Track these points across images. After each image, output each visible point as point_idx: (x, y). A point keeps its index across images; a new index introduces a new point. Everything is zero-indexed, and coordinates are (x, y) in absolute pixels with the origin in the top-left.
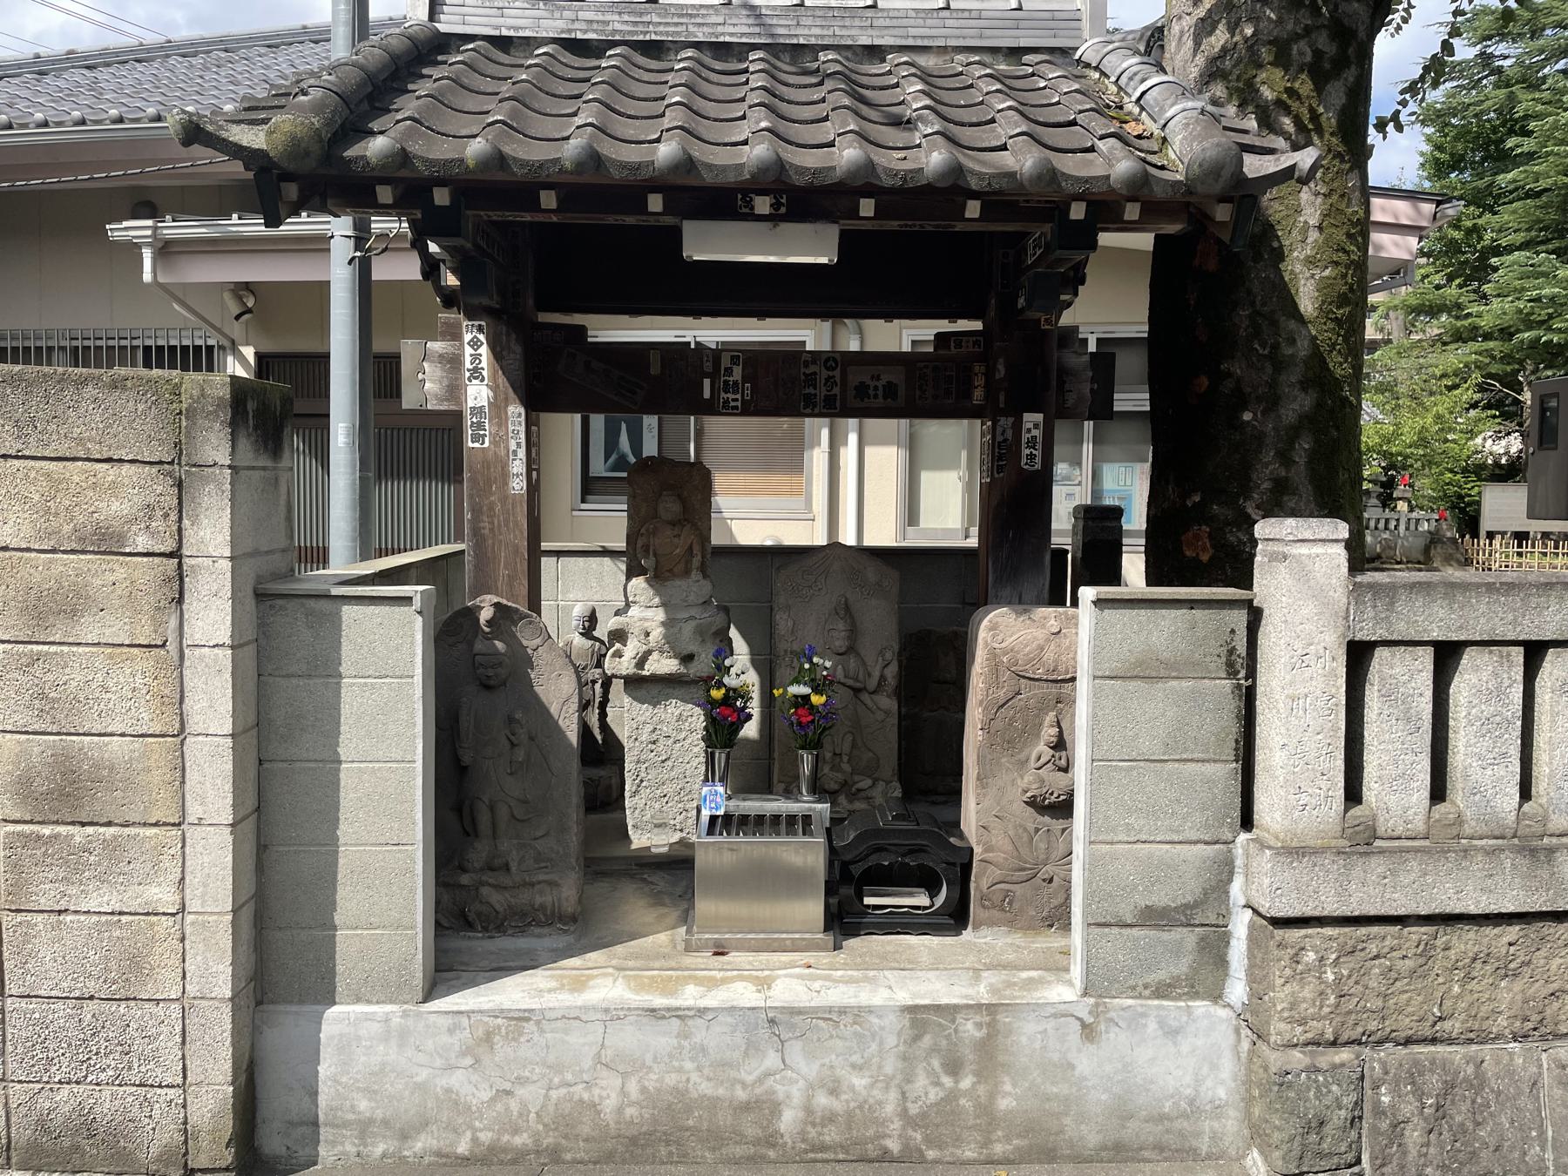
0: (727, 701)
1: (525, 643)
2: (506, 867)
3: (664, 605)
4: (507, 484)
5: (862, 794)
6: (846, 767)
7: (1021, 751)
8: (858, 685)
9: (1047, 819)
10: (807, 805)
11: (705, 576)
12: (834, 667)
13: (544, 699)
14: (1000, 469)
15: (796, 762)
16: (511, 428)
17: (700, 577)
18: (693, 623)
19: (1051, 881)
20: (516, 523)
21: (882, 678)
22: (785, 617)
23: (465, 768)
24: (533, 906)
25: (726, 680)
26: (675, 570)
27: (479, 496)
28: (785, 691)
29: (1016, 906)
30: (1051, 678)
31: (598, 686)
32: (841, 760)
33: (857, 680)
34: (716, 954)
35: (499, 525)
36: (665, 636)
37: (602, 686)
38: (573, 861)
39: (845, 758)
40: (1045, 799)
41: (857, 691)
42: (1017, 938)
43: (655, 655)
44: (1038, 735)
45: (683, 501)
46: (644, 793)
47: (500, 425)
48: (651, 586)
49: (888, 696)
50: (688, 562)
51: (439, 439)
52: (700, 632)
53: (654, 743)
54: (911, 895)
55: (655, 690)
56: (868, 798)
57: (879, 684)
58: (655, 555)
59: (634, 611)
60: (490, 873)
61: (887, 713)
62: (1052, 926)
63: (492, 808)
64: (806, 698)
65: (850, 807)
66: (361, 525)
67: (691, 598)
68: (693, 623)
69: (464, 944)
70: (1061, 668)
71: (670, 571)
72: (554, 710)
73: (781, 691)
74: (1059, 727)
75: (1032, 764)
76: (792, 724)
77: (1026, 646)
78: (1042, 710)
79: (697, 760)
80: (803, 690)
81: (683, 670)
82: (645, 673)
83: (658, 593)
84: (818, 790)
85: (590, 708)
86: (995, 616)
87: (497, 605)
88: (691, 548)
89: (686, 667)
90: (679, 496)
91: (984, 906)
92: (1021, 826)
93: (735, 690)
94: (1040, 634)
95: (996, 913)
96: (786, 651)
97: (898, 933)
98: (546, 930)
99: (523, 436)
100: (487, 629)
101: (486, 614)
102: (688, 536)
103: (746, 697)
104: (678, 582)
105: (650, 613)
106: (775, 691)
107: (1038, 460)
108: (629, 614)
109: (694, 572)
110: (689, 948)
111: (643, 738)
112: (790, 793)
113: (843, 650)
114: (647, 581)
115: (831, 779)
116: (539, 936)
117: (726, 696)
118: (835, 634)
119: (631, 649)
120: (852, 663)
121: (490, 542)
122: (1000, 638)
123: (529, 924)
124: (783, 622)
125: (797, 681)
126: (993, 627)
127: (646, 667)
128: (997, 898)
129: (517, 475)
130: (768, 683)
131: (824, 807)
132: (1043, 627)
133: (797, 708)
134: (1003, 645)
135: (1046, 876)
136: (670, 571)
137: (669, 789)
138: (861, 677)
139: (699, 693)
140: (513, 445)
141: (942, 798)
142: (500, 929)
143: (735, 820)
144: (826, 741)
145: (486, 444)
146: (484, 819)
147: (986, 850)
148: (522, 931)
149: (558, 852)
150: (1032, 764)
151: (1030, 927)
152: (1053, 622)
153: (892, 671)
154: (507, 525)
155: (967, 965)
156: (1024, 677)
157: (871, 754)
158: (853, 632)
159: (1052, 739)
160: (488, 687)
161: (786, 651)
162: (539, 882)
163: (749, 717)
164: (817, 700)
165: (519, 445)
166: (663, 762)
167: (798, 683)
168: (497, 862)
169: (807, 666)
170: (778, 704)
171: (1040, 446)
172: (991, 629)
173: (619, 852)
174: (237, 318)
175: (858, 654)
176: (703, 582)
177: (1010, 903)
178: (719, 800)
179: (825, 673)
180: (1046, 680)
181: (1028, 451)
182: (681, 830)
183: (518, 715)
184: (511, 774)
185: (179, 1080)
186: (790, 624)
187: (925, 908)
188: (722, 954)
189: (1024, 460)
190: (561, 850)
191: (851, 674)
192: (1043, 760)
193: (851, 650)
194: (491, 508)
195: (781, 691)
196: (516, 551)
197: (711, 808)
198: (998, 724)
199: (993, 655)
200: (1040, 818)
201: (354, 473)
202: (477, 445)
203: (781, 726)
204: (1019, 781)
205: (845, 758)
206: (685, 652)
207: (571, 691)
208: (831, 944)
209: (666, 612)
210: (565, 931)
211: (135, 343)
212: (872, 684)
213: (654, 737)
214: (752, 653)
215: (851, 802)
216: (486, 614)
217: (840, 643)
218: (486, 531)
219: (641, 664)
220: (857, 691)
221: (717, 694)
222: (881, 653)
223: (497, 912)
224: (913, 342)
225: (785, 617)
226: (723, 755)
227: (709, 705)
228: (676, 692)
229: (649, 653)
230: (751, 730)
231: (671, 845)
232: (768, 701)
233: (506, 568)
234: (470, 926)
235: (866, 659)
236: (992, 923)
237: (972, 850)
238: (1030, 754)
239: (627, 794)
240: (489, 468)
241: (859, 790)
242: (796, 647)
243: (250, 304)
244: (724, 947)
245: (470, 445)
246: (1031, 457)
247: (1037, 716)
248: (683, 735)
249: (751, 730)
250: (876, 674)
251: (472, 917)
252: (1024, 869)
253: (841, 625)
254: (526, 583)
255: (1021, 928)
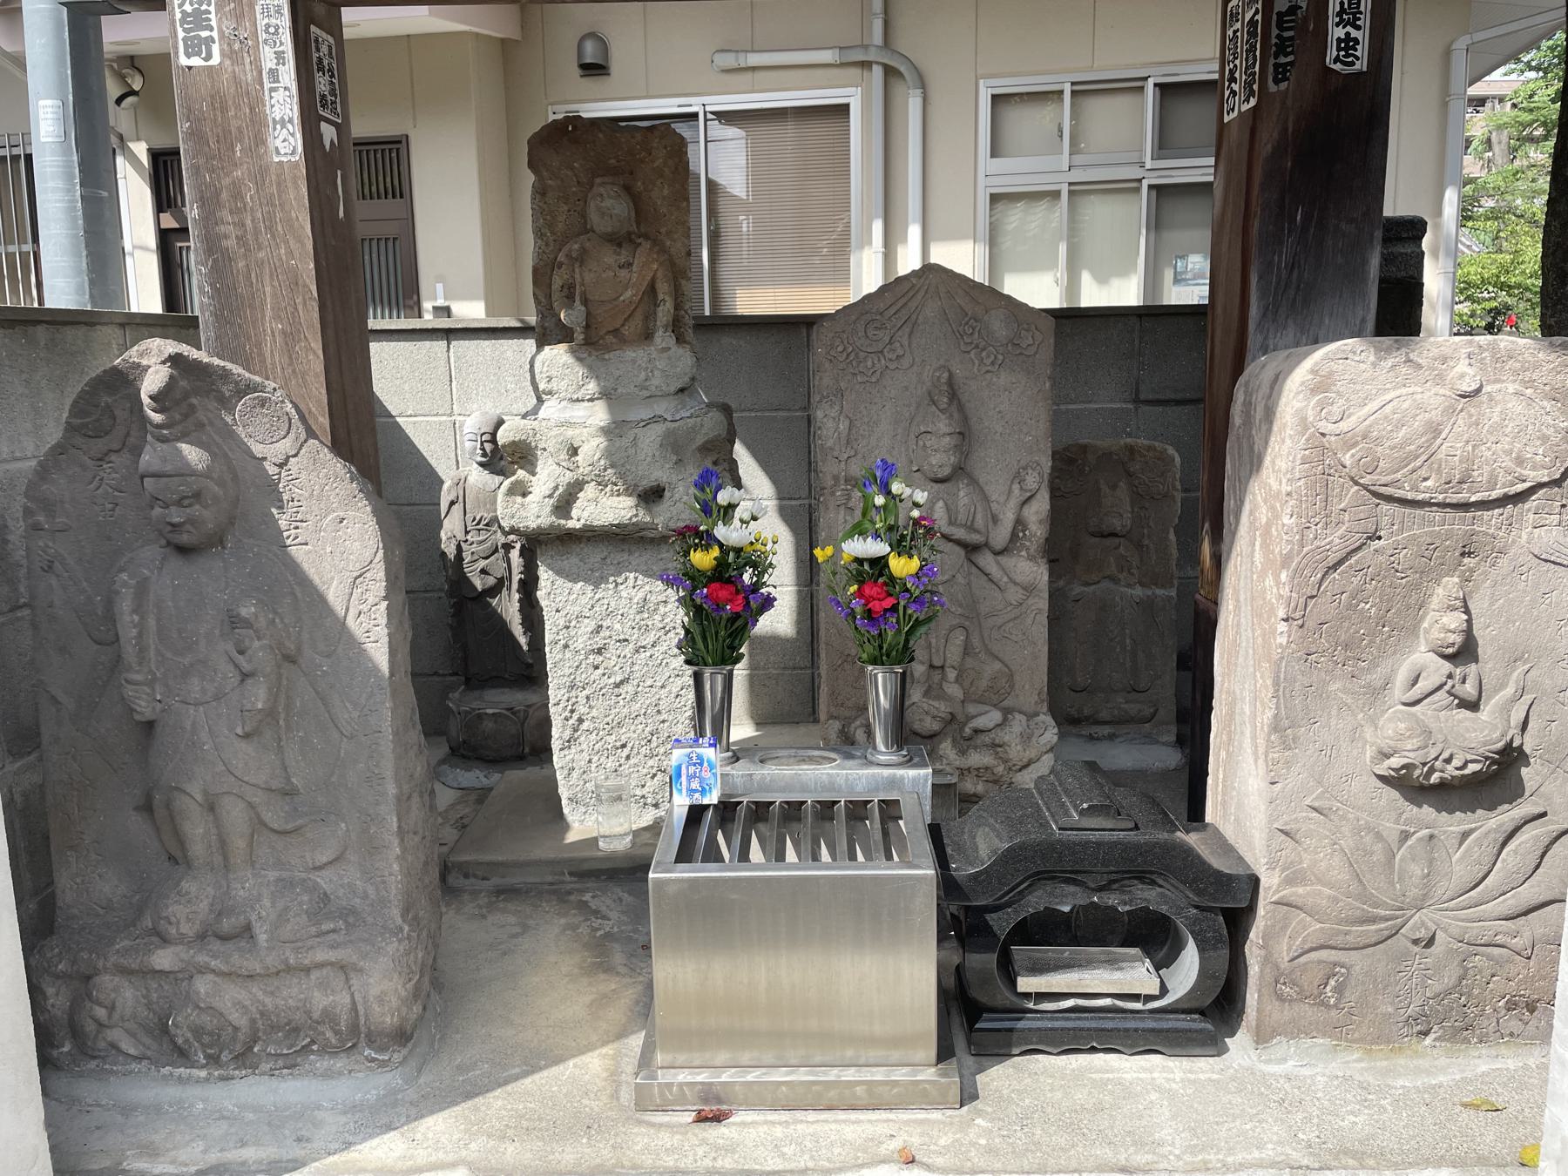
0: (723, 574)
1: (258, 449)
2: (247, 932)
3: (606, 395)
4: (264, 142)
5: (986, 739)
6: (954, 690)
7: (1374, 665)
8: (975, 538)
9: (1427, 811)
10: (887, 772)
11: (680, 340)
12: (932, 502)
13: (316, 580)
14: (1281, 73)
15: (860, 685)
16: (262, 22)
17: (671, 341)
18: (659, 429)
19: (1430, 942)
20: (289, 222)
21: (1020, 523)
22: (833, 413)
23: (150, 725)
24: (308, 1013)
25: (720, 532)
26: (626, 331)
27: (212, 171)
28: (838, 551)
29: (1351, 996)
30: (1454, 498)
31: (515, 555)
32: (944, 678)
33: (971, 528)
34: (702, 1118)
35: (256, 232)
36: (608, 453)
37: (522, 554)
38: (396, 913)
39: (952, 675)
40: (1432, 770)
41: (971, 549)
42: (1352, 1063)
43: (590, 490)
44: (1413, 631)
45: (636, 200)
46: (585, 742)
47: (239, 17)
48: (579, 359)
49: (1031, 558)
50: (649, 317)
51: (383, 258)
52: (674, 446)
53: (599, 652)
54: (1113, 963)
55: (595, 554)
56: (995, 745)
57: (1014, 536)
58: (585, 302)
59: (550, 409)
60: (216, 945)
61: (1029, 589)
62: (1426, 1033)
63: (211, 807)
64: (879, 563)
65: (959, 762)
66: (92, 282)
67: (655, 382)
68: (659, 429)
69: (172, 1092)
70: (1478, 475)
71: (615, 332)
72: (335, 595)
73: (829, 550)
74: (1467, 611)
75: (1398, 691)
76: (852, 614)
77: (1400, 425)
78: (1428, 569)
79: (679, 682)
80: (874, 547)
81: (643, 517)
82: (572, 524)
83: (594, 372)
84: (907, 737)
85: (505, 592)
86: (1326, 358)
87: (175, 360)
88: (652, 289)
89: (649, 511)
90: (627, 189)
91: (1281, 998)
92: (1369, 829)
93: (738, 551)
94: (1433, 398)
95: (1307, 1011)
96: (836, 478)
97: (1093, 1050)
98: (340, 1063)
99: (286, 37)
100: (157, 418)
101: (153, 380)
102: (644, 266)
103: (761, 566)
104: (630, 354)
105: (579, 412)
106: (818, 552)
107: (1362, 51)
108: (542, 414)
109: (660, 333)
110: (646, 1102)
111: (580, 643)
112: (849, 743)
113: (946, 471)
114: (573, 351)
115: (926, 713)
116: (328, 1075)
117: (721, 564)
118: (931, 442)
119: (546, 478)
120: (963, 495)
121: (241, 264)
122: (1336, 410)
123: (306, 1050)
124: (830, 423)
125: (859, 531)
126: (1321, 385)
127: (575, 513)
128: (1310, 981)
129: (283, 123)
130: (807, 532)
131: (919, 778)
132: (1440, 379)
133: (861, 583)
134: (1344, 426)
135: (1422, 934)
136: (615, 332)
137: (629, 733)
138: (980, 522)
139: (669, 559)
140: (269, 62)
141: (1106, 730)
142: (245, 1059)
143: (741, 812)
144: (919, 647)
145: (216, 60)
146: (197, 830)
147: (1289, 881)
148: (290, 1063)
149: (366, 896)
150: (1398, 691)
151: (1381, 1038)
152: (1462, 367)
153: (1039, 509)
154: (270, 228)
155: (1269, 1152)
156: (1390, 499)
157: (997, 666)
158: (965, 437)
159: (1452, 638)
160: (183, 550)
161: (836, 478)
162: (320, 966)
163: (768, 602)
164: (902, 566)
165: (280, 56)
166: (617, 685)
167: (863, 533)
168: (227, 925)
169: (880, 500)
170: (823, 577)
171: (1365, 20)
172: (1314, 391)
173: (543, 850)
174: (119, 101)
175: (973, 481)
176: (677, 351)
177: (1339, 990)
178: (707, 775)
179: (916, 513)
180: (1443, 505)
181: (1340, 32)
182: (656, 806)
183: (247, 610)
184: (247, 736)
185: (1142, 397)
186: (843, 426)
187: (1149, 998)
188: (718, 1118)
189: (1332, 52)
190: (371, 891)
191: (962, 518)
192: (1424, 685)
193: (960, 471)
194: (237, 195)
195: (829, 550)
196: (295, 283)
197: (691, 791)
198: (1324, 607)
199: (1319, 448)
200: (1411, 810)
201: (70, 191)
202: (196, 61)
203: (829, 617)
204: (1368, 733)
205: (952, 675)
206: (645, 484)
207: (368, 554)
208: (955, 1092)
209: (611, 409)
210: (383, 1064)
211: (15, 151)
212: (1000, 536)
213: (599, 641)
214: (781, 496)
215: (963, 752)
216: (153, 380)
217: (941, 461)
218: (231, 243)
219: (564, 505)
220: (971, 549)
221: (703, 559)
222: (1018, 477)
223: (236, 1029)
224: (994, 96)
225: (833, 413)
226: (719, 678)
227: (691, 579)
228: (635, 559)
229: (576, 487)
230: (779, 620)
231: (636, 833)
232: (808, 570)
233: (277, 318)
234: (182, 1055)
235: (989, 489)
236: (1295, 1031)
237: (1255, 881)
238: (1394, 671)
239: (555, 745)
240: (224, 110)
241: (977, 731)
242: (856, 469)
243: (136, 87)
244: (719, 1101)
245: (184, 61)
246: (1348, 44)
247: (1417, 586)
248: (651, 638)
249: (779, 620)
250: (1008, 518)
251: (182, 1036)
252: (1373, 920)
253: (943, 425)
254: (317, 346)
255: (1361, 1040)
